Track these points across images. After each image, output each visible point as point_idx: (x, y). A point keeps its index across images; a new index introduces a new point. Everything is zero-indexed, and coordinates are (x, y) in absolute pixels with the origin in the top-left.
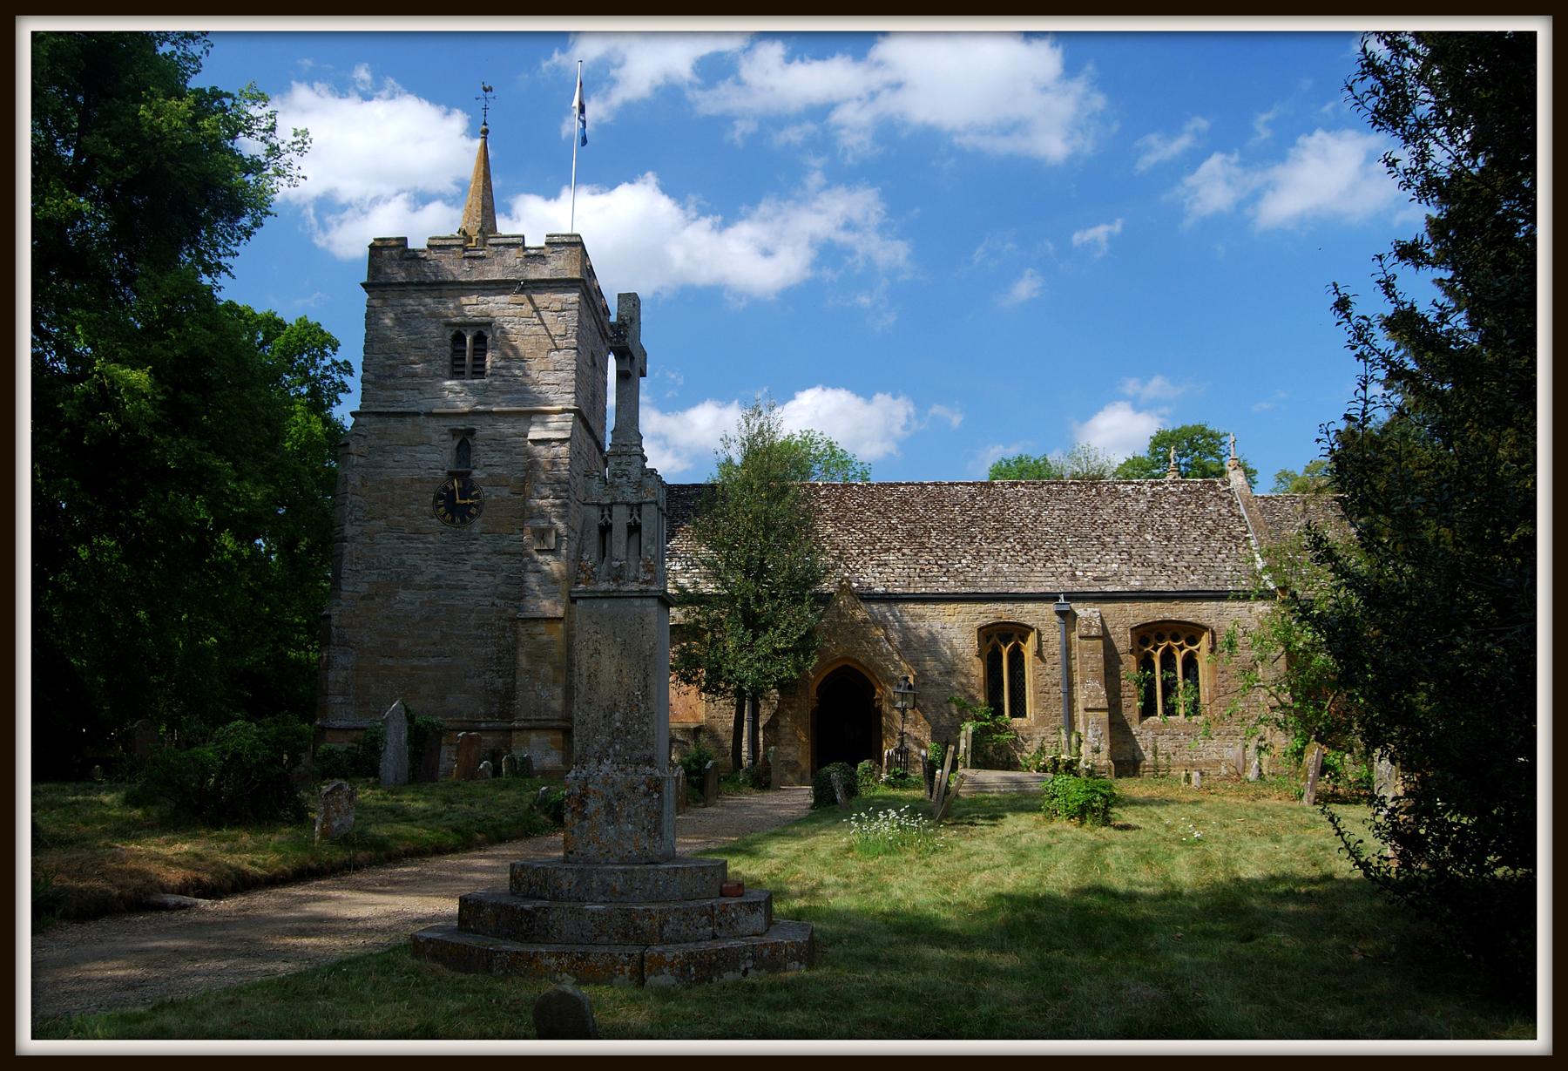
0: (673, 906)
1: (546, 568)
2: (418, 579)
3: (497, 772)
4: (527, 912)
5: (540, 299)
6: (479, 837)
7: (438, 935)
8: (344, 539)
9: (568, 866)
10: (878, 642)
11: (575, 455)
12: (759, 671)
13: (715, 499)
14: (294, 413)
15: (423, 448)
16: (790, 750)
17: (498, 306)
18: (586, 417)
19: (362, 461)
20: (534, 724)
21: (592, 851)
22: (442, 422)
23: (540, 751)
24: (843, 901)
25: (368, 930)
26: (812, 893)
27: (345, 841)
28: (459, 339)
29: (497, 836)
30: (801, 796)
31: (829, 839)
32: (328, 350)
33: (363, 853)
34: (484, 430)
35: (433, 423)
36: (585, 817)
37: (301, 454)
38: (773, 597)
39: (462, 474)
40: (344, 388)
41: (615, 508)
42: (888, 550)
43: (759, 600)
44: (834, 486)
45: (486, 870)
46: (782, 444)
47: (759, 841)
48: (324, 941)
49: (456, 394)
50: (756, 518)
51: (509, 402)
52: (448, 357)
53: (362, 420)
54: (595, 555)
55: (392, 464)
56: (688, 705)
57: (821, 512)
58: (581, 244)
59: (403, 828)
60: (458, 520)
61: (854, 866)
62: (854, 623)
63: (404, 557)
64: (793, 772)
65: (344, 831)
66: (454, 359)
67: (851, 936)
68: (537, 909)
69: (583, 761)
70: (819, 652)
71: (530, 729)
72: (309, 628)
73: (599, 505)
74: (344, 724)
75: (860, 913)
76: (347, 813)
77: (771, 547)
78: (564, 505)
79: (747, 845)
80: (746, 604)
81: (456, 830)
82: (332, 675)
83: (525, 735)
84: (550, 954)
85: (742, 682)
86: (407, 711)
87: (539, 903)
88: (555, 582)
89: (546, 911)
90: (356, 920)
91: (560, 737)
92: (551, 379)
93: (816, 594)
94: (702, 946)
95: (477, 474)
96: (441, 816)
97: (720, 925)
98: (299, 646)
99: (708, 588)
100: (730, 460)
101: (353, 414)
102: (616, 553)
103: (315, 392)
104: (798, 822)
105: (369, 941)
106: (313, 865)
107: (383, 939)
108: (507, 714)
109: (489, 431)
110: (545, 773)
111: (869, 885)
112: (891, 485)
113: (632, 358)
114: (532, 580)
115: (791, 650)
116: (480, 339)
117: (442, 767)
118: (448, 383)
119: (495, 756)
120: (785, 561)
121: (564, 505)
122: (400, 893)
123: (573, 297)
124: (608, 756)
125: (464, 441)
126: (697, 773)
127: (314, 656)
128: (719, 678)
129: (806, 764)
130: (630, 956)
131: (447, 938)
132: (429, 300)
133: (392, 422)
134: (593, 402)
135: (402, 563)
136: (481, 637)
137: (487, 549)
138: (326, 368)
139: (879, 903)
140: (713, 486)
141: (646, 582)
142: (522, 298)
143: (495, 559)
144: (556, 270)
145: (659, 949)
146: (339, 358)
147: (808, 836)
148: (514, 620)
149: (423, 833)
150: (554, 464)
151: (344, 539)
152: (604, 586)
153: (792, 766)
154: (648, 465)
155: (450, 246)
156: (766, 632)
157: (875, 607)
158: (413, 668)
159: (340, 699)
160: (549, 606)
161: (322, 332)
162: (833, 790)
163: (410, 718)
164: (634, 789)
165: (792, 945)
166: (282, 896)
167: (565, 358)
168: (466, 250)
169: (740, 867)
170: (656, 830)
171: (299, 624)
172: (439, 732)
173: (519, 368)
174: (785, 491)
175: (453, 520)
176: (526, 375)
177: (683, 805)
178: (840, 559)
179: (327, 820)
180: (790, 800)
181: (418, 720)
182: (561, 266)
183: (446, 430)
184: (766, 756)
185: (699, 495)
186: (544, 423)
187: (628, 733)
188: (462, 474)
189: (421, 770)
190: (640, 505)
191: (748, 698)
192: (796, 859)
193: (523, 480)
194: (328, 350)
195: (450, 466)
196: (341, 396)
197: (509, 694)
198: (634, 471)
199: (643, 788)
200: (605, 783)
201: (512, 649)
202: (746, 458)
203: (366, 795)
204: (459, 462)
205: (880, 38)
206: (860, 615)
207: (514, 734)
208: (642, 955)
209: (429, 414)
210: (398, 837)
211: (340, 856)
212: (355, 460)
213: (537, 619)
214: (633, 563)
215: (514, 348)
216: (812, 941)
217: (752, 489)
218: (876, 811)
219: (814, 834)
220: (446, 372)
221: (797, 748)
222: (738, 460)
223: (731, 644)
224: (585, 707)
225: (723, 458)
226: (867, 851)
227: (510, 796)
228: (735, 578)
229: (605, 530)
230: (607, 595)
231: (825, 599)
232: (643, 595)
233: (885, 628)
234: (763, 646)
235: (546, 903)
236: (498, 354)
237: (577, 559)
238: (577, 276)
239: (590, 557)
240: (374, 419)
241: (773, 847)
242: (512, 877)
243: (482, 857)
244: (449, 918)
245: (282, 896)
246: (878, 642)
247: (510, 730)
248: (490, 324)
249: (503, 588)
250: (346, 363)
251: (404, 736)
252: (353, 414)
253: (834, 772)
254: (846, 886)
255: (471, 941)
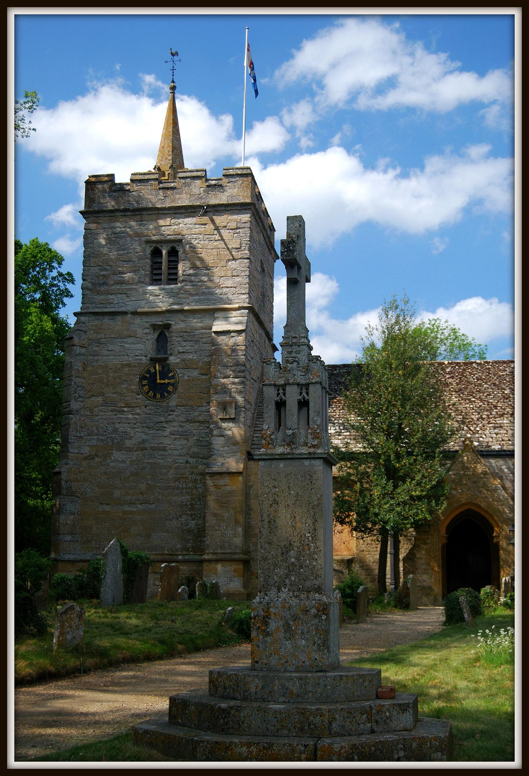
0: (339, 706)
1: (229, 433)
2: (128, 443)
3: (192, 595)
4: (224, 710)
5: (220, 220)
6: (180, 647)
7: (153, 728)
8: (70, 412)
9: (255, 673)
10: (495, 490)
11: (250, 343)
12: (399, 514)
13: (362, 376)
14: (30, 314)
15: (130, 340)
16: (425, 577)
17: (187, 227)
18: (259, 312)
19: (83, 350)
20: (220, 556)
21: (274, 661)
22: (145, 319)
23: (225, 578)
24: (473, 703)
25: (97, 723)
26: (447, 696)
27: (77, 650)
28: (156, 253)
29: (194, 647)
30: (434, 615)
31: (460, 651)
32: (55, 265)
33: (90, 660)
34: (178, 325)
35: (138, 320)
36: (268, 634)
37: (36, 346)
38: (410, 454)
39: (160, 360)
40: (68, 294)
41: (288, 388)
42: (502, 415)
43: (398, 456)
44: (457, 364)
45: (190, 674)
46: (415, 331)
47: (404, 652)
48: (63, 731)
49: (158, 297)
50: (394, 391)
51: (199, 302)
52: (148, 268)
53: (83, 319)
54: (272, 425)
55: (106, 353)
56: (345, 542)
57: (447, 385)
58: (251, 175)
59: (121, 641)
60: (158, 396)
61: (481, 673)
62: (475, 474)
63: (117, 426)
64: (427, 595)
65: (76, 642)
66: (153, 269)
67: (482, 732)
68: (231, 708)
69: (265, 589)
70: (447, 498)
71: (217, 561)
72: (44, 481)
73: (275, 385)
74: (72, 557)
75: (490, 713)
76: (78, 628)
77: (408, 414)
78: (242, 383)
79: (393, 655)
80: (388, 460)
81: (162, 642)
82: (62, 518)
83: (212, 566)
84: (242, 744)
85: (386, 523)
86: (122, 547)
87: (232, 703)
88: (236, 443)
89: (238, 709)
90: (86, 714)
91: (241, 567)
92: (229, 283)
93: (444, 452)
94: (363, 739)
95: (172, 359)
96: (149, 630)
97: (377, 722)
98: (36, 496)
99: (358, 447)
100: (373, 345)
101: (75, 314)
102: (289, 424)
103: (45, 298)
104: (432, 636)
105: (98, 732)
106: (52, 669)
107: (109, 730)
108: (199, 549)
109: (182, 325)
110: (230, 595)
111: (494, 690)
112: (504, 362)
113: (299, 268)
114: (218, 442)
115: (425, 497)
116: (173, 253)
117: (149, 590)
118: (150, 288)
119: (190, 582)
120: (419, 425)
121: (242, 383)
122: (120, 692)
123: (246, 217)
124: (285, 586)
125: (162, 333)
126: (351, 596)
127: (47, 504)
128: (367, 520)
129: (438, 589)
130: (306, 746)
131: (160, 730)
132: (133, 223)
133: (106, 320)
134: (263, 301)
135: (115, 430)
136: (178, 488)
137: (182, 419)
138: (54, 278)
139: (503, 705)
140: (359, 366)
141: (313, 446)
142: (206, 219)
143: (188, 426)
144: (232, 196)
145: (328, 741)
146: (64, 270)
147: (443, 647)
148: (203, 474)
149: (136, 645)
150: (234, 351)
151: (70, 412)
152: (280, 450)
153: (427, 590)
154: (314, 353)
155: (148, 180)
156: (404, 482)
157: (493, 461)
158: (125, 513)
159: (69, 538)
160: (234, 464)
161: (50, 250)
162: (461, 610)
163: (124, 553)
164: (306, 612)
165: (435, 739)
166: (29, 693)
167: (241, 266)
168: (160, 182)
169: (391, 673)
170: (325, 645)
171: (35, 479)
172: (147, 563)
173: (207, 275)
174: (417, 368)
175: (155, 396)
176: (211, 281)
177: (343, 620)
178: (463, 423)
179: (62, 634)
180: (426, 618)
181: (130, 554)
182: (234, 193)
183: (147, 325)
184: (405, 583)
185: (349, 373)
186: (226, 318)
187: (301, 567)
188: (160, 360)
189: (133, 592)
190: (307, 385)
191: (389, 536)
192: (433, 667)
193: (209, 364)
194: (55, 265)
195: (152, 354)
196: (66, 300)
197: (200, 533)
198: (303, 358)
199: (314, 611)
200: (283, 607)
201: (202, 498)
202: (386, 343)
203: (91, 613)
204: (158, 351)
205: (510, 73)
206: (480, 468)
207: (205, 565)
208: (315, 745)
209: (135, 313)
210: (117, 647)
211: (73, 662)
212: (78, 350)
213: (221, 474)
214: (303, 431)
215: (201, 260)
216: (451, 736)
217: (391, 368)
218: (498, 629)
219: (447, 646)
220: (147, 280)
221: (431, 576)
222: (379, 345)
223: (376, 492)
224: (267, 546)
225: (367, 343)
226: (492, 661)
227: (203, 615)
228: (379, 439)
229: (280, 405)
230: (283, 458)
231: (452, 455)
232: (311, 457)
233: (501, 478)
234: (403, 492)
235: (238, 703)
236: (188, 264)
237: (254, 426)
238: (248, 201)
239: (268, 426)
240: (92, 318)
241: (415, 658)
242: (211, 681)
243: (182, 664)
244: (159, 713)
245: (29, 693)
246: (495, 490)
247: (201, 562)
248: (180, 241)
249: (195, 449)
250: (69, 274)
251: (119, 566)
252: (75, 314)
253: (462, 596)
254: (476, 690)
255: (179, 732)
